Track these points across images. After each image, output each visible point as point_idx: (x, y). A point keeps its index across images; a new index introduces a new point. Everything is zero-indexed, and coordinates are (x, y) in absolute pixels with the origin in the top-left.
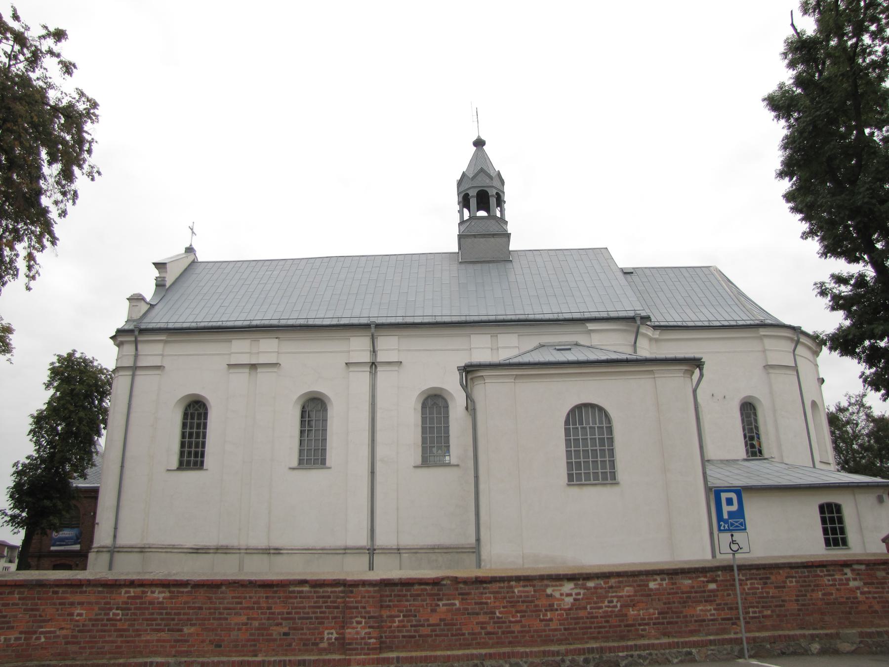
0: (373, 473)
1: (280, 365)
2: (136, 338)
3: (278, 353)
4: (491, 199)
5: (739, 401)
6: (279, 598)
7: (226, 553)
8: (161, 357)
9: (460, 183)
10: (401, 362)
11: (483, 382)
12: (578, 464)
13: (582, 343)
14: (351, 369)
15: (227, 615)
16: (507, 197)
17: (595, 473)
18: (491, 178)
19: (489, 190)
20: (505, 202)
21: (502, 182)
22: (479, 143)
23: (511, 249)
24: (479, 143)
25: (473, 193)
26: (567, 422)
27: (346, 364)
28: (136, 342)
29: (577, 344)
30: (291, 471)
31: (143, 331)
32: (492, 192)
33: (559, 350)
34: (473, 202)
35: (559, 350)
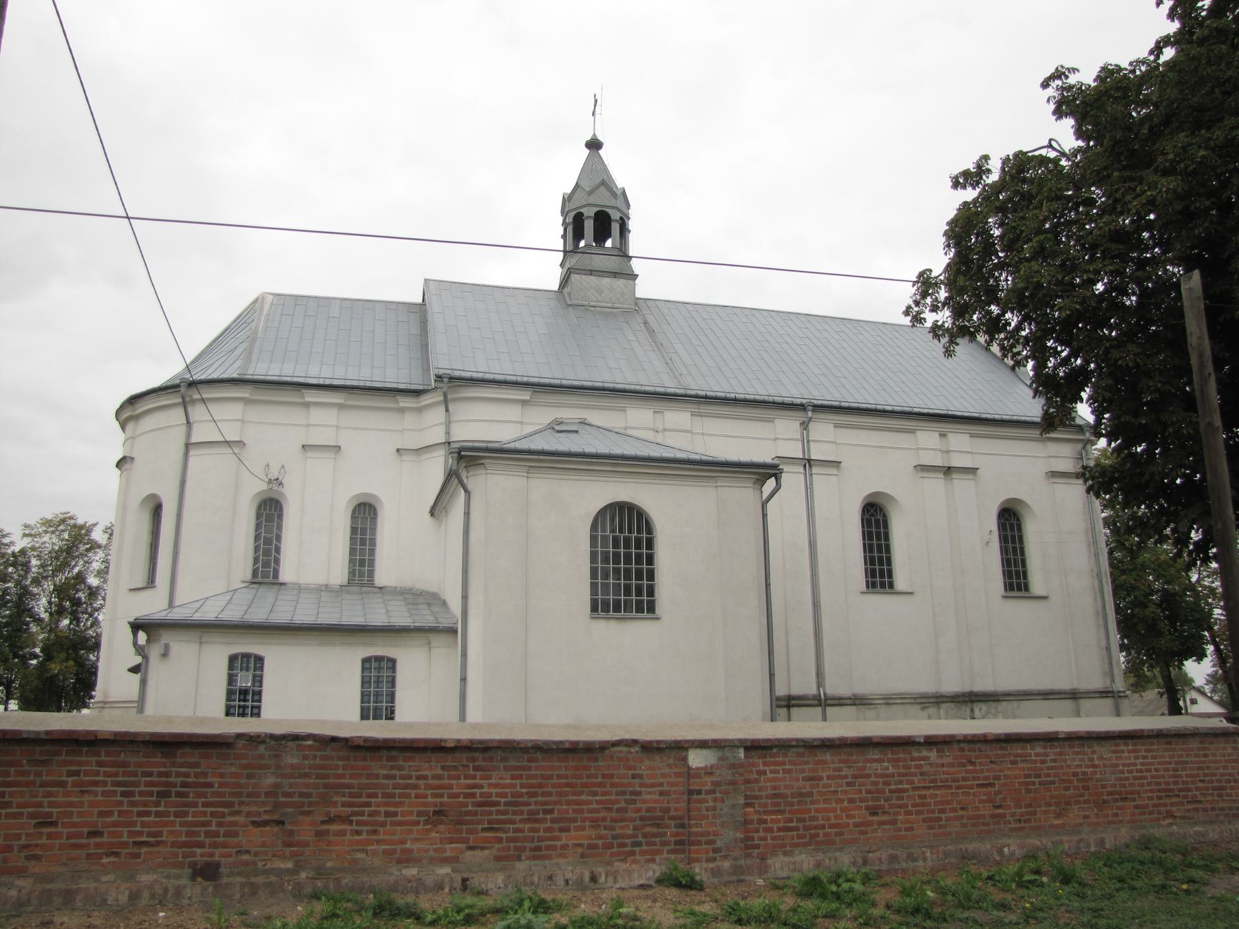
0: (768, 585)
1: (245, 444)
2: (183, 398)
3: (337, 427)
4: (586, 222)
5: (862, 498)
6: (1069, 766)
7: (969, 700)
8: (240, 423)
9: (567, 200)
10: (340, 447)
11: (484, 472)
12: (639, 576)
13: (593, 422)
14: (309, 454)
15: (115, 792)
16: (631, 225)
17: (881, 582)
18: (614, 195)
19: (609, 211)
20: (629, 231)
21: (628, 206)
22: (594, 145)
23: (638, 295)
24: (594, 145)
25: (589, 212)
26: (594, 527)
27: (303, 446)
28: (185, 404)
29: (583, 422)
30: (133, 594)
31: (192, 384)
32: (615, 215)
33: (559, 432)
34: (589, 226)
35: (559, 432)
